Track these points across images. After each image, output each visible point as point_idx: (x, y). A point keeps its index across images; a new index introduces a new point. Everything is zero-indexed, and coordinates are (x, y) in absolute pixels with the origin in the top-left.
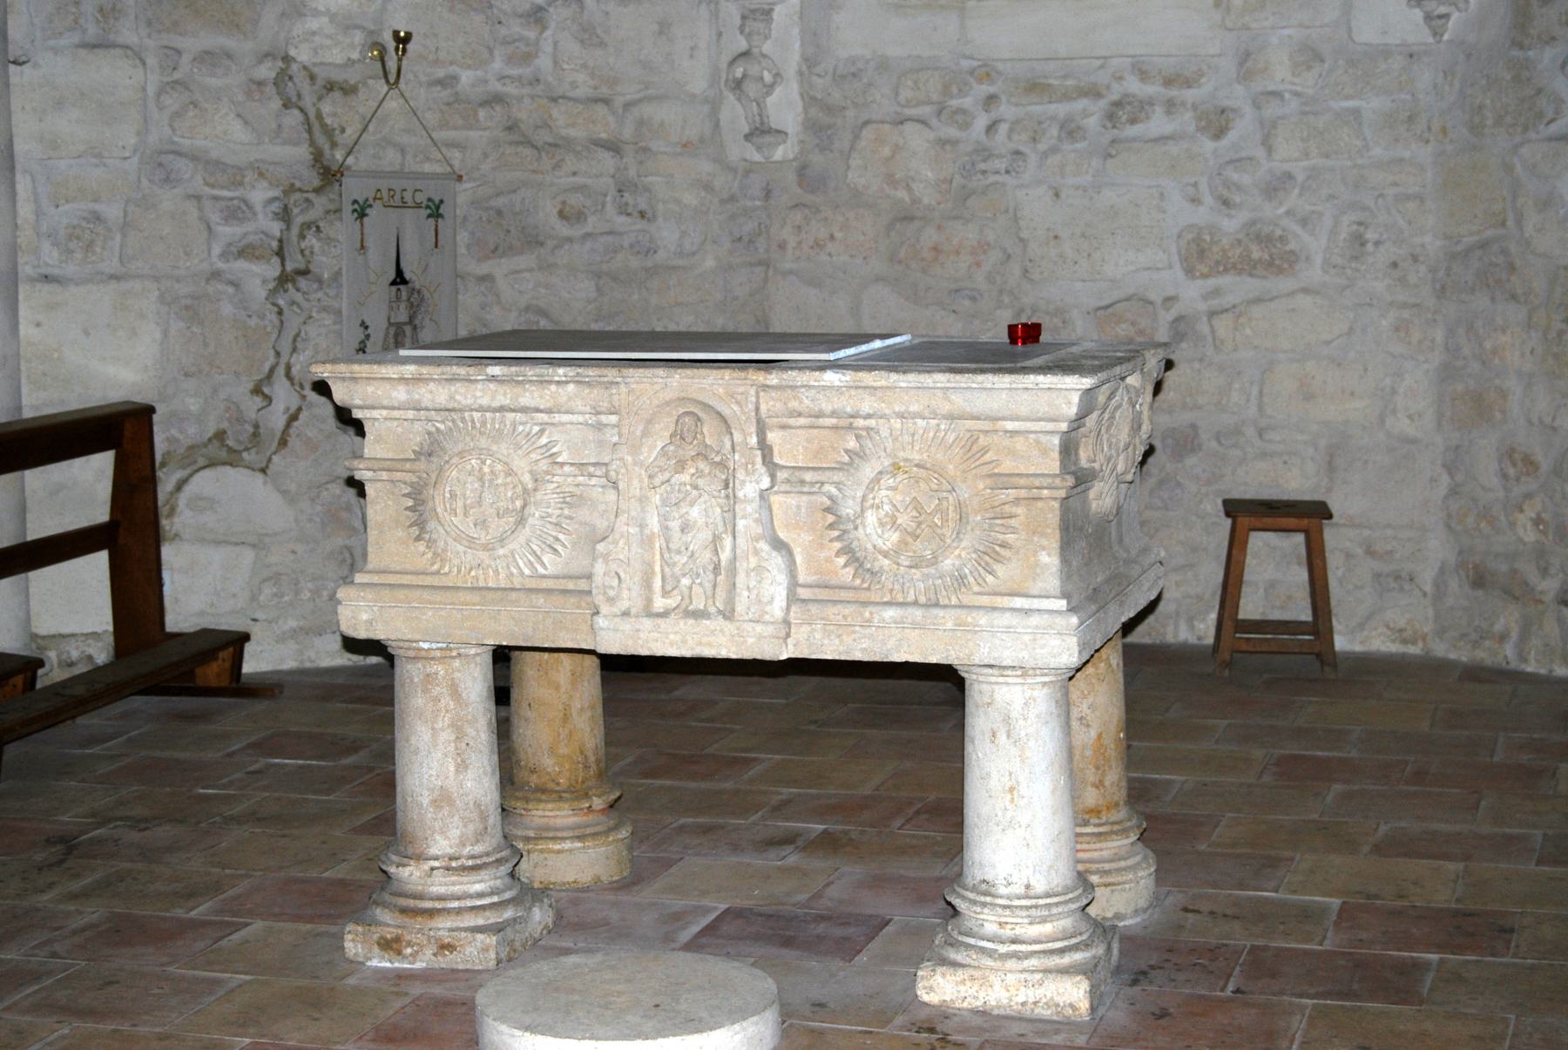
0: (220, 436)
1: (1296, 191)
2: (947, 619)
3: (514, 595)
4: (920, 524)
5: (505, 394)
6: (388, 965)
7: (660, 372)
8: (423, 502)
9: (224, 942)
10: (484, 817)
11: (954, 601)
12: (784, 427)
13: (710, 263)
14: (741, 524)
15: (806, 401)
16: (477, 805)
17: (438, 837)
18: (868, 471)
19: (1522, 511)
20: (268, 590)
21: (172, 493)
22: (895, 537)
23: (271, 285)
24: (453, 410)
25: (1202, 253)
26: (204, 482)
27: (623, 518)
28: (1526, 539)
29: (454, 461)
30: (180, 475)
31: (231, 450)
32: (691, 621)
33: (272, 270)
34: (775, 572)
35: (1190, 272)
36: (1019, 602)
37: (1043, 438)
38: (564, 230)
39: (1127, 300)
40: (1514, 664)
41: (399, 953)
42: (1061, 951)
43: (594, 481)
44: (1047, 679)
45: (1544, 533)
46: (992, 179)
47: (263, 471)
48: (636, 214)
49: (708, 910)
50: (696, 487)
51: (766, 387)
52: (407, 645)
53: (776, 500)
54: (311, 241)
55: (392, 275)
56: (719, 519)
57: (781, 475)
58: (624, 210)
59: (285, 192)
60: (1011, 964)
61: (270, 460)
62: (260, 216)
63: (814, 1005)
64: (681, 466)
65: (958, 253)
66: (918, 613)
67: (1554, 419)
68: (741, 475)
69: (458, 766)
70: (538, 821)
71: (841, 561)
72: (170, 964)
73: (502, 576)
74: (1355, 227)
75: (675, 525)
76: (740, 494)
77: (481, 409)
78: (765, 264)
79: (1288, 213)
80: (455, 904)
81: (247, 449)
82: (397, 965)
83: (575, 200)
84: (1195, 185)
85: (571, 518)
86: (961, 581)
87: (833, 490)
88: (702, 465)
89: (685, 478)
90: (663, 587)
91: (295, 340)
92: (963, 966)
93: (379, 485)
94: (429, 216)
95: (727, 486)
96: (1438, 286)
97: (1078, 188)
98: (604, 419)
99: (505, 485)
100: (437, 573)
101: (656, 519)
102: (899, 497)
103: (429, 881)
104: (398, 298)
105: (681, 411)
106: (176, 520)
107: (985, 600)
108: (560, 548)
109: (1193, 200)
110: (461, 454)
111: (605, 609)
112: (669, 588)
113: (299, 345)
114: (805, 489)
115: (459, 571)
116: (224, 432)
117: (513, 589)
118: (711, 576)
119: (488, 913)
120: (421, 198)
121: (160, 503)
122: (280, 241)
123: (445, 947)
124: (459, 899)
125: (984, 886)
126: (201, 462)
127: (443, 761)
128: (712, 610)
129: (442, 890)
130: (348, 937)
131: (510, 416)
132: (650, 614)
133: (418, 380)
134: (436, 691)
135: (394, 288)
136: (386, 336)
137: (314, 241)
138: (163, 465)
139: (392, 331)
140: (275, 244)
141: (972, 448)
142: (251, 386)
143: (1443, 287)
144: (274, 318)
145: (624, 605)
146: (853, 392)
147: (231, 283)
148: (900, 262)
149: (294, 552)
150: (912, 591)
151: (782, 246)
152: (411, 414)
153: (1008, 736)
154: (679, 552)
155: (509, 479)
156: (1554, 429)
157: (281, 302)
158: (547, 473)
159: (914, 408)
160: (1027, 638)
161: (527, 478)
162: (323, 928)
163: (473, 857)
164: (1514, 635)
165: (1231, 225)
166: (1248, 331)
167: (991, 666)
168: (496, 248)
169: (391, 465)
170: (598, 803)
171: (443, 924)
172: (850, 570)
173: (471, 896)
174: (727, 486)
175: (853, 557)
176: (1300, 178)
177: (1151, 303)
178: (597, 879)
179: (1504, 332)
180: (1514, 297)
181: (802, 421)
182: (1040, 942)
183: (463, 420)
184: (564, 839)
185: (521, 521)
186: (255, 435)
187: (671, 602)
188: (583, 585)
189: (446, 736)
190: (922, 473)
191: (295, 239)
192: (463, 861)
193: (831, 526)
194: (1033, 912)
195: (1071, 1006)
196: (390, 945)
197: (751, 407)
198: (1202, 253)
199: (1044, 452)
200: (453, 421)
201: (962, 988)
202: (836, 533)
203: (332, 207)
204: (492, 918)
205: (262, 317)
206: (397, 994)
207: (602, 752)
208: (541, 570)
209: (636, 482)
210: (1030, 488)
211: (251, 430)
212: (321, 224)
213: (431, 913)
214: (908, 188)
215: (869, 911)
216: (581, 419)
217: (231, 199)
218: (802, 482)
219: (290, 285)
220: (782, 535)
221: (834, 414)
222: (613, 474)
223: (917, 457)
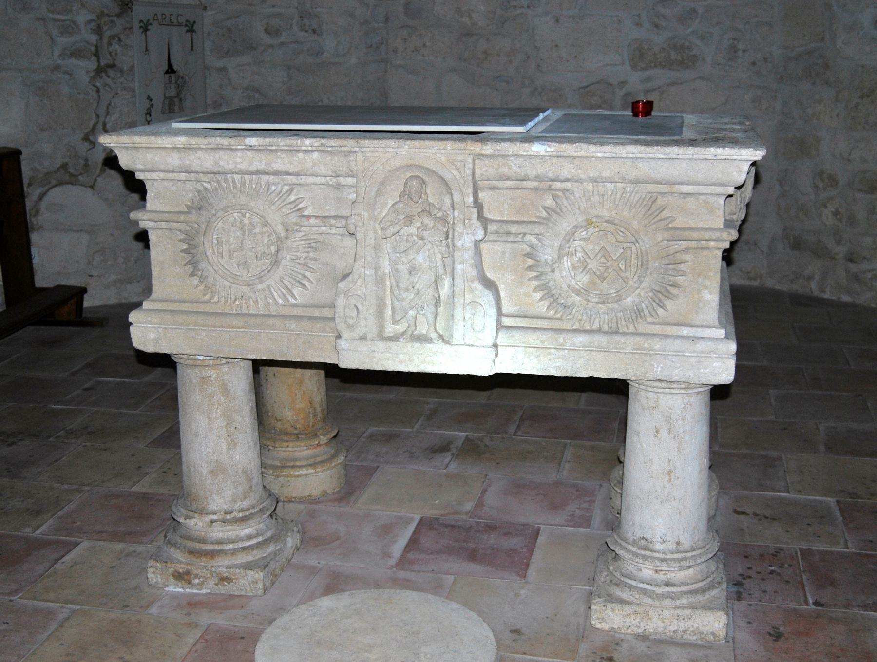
0: (64, 166)
1: (697, 21)
2: (628, 343)
3: (271, 321)
4: (607, 268)
5: (260, 161)
6: (181, 590)
7: (392, 143)
8: (196, 247)
9: (58, 566)
10: (249, 480)
11: (632, 329)
12: (493, 188)
13: (354, 60)
14: (459, 267)
15: (514, 167)
16: (244, 471)
17: (215, 497)
18: (565, 225)
19: (826, 207)
20: (98, 258)
21: (36, 202)
22: (585, 278)
23: (92, 74)
24: (219, 173)
25: (642, 56)
26: (56, 195)
27: (360, 263)
28: (827, 223)
29: (219, 214)
30: (39, 191)
31: (71, 175)
32: (417, 345)
33: (92, 65)
34: (487, 307)
35: (634, 67)
36: (685, 331)
37: (712, 199)
38: (268, 40)
39: (598, 83)
40: (816, 293)
41: (189, 582)
42: (703, 591)
43: (334, 231)
44: (699, 390)
45: (840, 220)
46: (519, 11)
47: (92, 187)
48: (310, 31)
49: (408, 521)
50: (422, 239)
51: (481, 156)
52: (185, 357)
53: (483, 246)
54: (116, 47)
55: (166, 67)
56: (440, 264)
57: (492, 227)
58: (303, 29)
59: (98, 16)
60: (668, 602)
61: (96, 180)
62: (83, 31)
63: (512, 631)
64: (409, 220)
65: (498, 55)
66: (603, 340)
67: (850, 155)
68: (459, 228)
69: (229, 445)
70: (282, 455)
71: (538, 295)
72: (16, 592)
73: (261, 305)
74: (732, 41)
75: (403, 268)
76: (459, 244)
77: (241, 172)
78: (386, 61)
79: (693, 32)
80: (231, 546)
81: (81, 174)
82: (188, 590)
83: (275, 22)
84: (639, 15)
85: (315, 260)
86: (638, 313)
87: (534, 240)
88: (426, 220)
89: (413, 230)
90: (393, 317)
91: (108, 108)
92: (628, 603)
93: (160, 232)
94: (187, 31)
95: (447, 237)
96: (778, 76)
97: (569, 17)
98: (342, 180)
99: (262, 233)
100: (209, 301)
101: (387, 262)
102: (590, 247)
103: (210, 529)
104: (170, 82)
105: (409, 175)
106: (40, 218)
107: (657, 329)
108: (307, 283)
109: (637, 25)
110: (225, 209)
111: (345, 334)
112: (398, 318)
113: (111, 111)
114: (510, 239)
115: (226, 301)
116: (67, 164)
117: (270, 316)
118: (433, 309)
119: (255, 552)
120: (182, 19)
121: (28, 208)
122: (96, 47)
123: (223, 579)
124: (233, 542)
125: (643, 542)
126: (54, 182)
127: (216, 436)
128: (434, 335)
129: (220, 535)
130: (150, 570)
131: (265, 178)
132: (382, 337)
133: (188, 149)
134: (211, 389)
135: (167, 76)
136: (164, 103)
137: (117, 46)
138: (30, 185)
139: (167, 102)
140: (93, 49)
141: (652, 208)
142: (82, 136)
143: (782, 77)
144: (95, 94)
145: (361, 331)
146: (555, 160)
147: (66, 73)
148: (465, 60)
149: (112, 235)
150: (597, 322)
151: (395, 51)
152: (183, 176)
153: (669, 432)
154: (407, 290)
155: (265, 229)
156: (849, 160)
157: (98, 84)
158: (296, 224)
159: (606, 174)
160: (693, 360)
161: (280, 229)
162: (131, 548)
163: (242, 510)
164: (817, 277)
165: (659, 39)
166: (667, 102)
167: (660, 381)
168: (228, 52)
169: (169, 217)
170: (324, 440)
171: (222, 564)
172: (546, 303)
173: (242, 539)
174: (447, 237)
175: (548, 293)
176: (700, 11)
177: (611, 85)
178: (325, 494)
179: (820, 104)
180: (827, 83)
181: (508, 183)
182: (688, 584)
183: (226, 181)
184: (301, 467)
185: (276, 263)
186: (86, 165)
187: (400, 328)
188: (327, 313)
189: (220, 423)
190: (610, 227)
191: (106, 46)
192: (235, 514)
193: (530, 268)
194: (684, 563)
195: (713, 634)
196: (182, 577)
197: (469, 172)
198: (642, 56)
199: (711, 211)
200: (218, 182)
201: (628, 620)
202: (535, 274)
203: (128, 26)
204: (257, 554)
205: (87, 94)
206: (189, 625)
207: (325, 406)
208: (292, 300)
209: (371, 234)
210: (699, 240)
211: (82, 162)
212: (122, 36)
213: (212, 554)
214: (470, 17)
215: (522, 520)
216: (323, 180)
217: (64, 21)
218: (508, 233)
219: (103, 74)
220: (490, 275)
221: (537, 178)
222: (352, 227)
223: (606, 214)
